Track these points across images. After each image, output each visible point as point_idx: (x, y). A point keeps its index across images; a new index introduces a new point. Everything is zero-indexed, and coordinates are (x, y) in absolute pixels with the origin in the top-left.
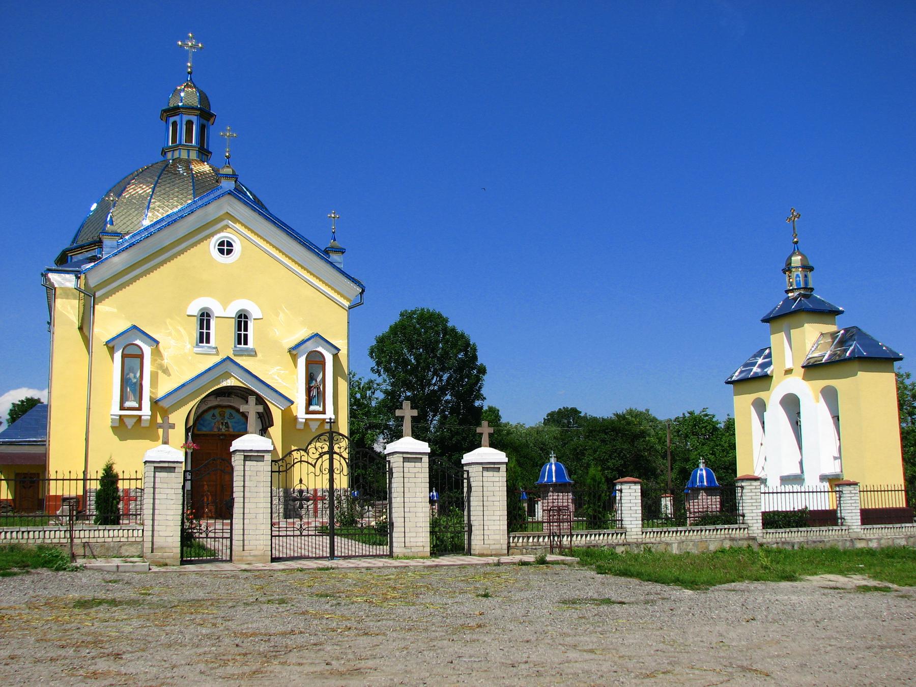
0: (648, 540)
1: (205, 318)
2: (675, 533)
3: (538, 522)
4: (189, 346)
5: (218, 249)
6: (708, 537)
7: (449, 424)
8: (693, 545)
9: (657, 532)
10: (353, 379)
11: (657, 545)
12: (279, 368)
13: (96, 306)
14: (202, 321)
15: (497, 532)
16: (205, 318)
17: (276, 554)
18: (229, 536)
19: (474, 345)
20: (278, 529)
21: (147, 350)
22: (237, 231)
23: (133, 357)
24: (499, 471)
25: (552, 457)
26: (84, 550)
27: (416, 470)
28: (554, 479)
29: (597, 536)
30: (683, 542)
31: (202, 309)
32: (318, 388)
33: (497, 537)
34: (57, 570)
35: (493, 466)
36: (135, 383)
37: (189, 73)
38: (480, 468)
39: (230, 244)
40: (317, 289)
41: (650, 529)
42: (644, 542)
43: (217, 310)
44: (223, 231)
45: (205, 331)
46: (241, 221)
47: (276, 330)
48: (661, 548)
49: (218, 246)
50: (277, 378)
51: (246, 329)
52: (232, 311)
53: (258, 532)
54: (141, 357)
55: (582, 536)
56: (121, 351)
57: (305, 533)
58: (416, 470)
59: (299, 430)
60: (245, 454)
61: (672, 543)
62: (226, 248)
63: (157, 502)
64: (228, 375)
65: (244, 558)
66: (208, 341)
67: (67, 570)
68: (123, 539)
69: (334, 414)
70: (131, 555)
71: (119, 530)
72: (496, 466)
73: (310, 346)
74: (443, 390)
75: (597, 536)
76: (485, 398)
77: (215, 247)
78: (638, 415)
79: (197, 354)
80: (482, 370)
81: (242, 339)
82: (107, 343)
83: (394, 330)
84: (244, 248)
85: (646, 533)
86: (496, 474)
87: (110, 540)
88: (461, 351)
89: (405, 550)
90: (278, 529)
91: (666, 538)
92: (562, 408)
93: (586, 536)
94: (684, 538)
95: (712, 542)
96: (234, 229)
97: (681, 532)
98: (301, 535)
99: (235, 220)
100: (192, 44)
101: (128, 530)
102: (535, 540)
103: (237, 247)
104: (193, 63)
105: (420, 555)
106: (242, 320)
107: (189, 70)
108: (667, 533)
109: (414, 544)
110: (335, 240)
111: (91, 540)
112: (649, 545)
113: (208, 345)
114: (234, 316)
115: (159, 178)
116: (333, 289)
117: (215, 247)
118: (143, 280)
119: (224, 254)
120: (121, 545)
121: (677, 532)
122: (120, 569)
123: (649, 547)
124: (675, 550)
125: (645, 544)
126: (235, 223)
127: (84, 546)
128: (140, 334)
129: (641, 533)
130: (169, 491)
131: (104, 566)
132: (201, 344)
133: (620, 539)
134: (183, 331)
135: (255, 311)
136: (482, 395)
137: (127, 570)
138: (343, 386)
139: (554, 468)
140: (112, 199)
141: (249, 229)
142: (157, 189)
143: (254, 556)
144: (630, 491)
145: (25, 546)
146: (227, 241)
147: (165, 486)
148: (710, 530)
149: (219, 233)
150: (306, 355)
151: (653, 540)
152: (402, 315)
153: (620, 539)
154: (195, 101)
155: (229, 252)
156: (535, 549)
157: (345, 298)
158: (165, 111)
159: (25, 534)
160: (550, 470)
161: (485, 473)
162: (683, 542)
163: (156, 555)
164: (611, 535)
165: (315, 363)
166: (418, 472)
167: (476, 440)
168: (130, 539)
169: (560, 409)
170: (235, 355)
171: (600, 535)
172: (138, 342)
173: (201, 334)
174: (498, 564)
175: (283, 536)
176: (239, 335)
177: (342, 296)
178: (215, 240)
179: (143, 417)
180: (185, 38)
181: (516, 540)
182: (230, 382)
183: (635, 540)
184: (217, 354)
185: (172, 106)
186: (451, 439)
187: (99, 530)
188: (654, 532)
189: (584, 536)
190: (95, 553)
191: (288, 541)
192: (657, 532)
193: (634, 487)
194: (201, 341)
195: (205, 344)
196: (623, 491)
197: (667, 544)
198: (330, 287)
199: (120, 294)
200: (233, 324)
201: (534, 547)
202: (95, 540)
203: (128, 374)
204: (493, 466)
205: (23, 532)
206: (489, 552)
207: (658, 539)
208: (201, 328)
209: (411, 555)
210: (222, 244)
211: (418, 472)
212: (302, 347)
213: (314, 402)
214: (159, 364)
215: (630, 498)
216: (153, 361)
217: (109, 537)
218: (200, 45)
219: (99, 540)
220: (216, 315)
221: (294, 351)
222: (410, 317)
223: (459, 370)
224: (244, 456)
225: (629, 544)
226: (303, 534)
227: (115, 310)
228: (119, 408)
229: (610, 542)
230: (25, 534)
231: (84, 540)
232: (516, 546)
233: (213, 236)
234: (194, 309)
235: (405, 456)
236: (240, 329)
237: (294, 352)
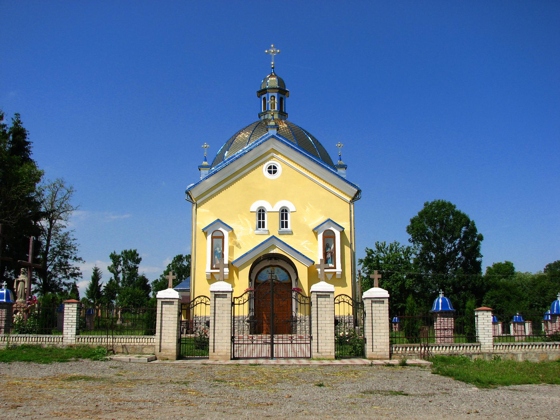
0: (498, 351)
1: (261, 213)
2: (448, 348)
3: (510, 336)
4: (251, 230)
5: (268, 171)
6: (548, 350)
7: (458, 273)
8: (535, 356)
9: (506, 346)
10: (398, 247)
11: (505, 355)
12: (307, 241)
13: (197, 209)
14: (259, 215)
15: (383, 344)
16: (261, 213)
17: (237, 355)
18: (309, 342)
19: (473, 222)
20: (277, 339)
21: (226, 233)
22: (279, 159)
23: (218, 238)
24: (384, 303)
25: (441, 293)
26: (123, 349)
27: (326, 303)
28: (440, 308)
29: (458, 347)
30: (527, 353)
31: (282, 207)
32: (331, 253)
33: (383, 347)
34: (94, 360)
35: (379, 300)
36: (220, 254)
37: (272, 68)
38: (370, 301)
39: (275, 167)
40: (330, 191)
41: (500, 344)
42: (495, 352)
43: (268, 207)
44: (270, 160)
45: (261, 221)
46: (281, 153)
47: (305, 218)
48: (509, 357)
49: (268, 169)
50: (306, 248)
51: (286, 218)
52: (277, 208)
53: (223, 341)
54: (223, 238)
55: (446, 347)
56: (211, 235)
57: (294, 342)
58: (326, 303)
59: (338, 279)
60: (215, 293)
61: (517, 354)
62: (272, 170)
63: (163, 322)
64: (274, 247)
65: (214, 357)
66: (264, 227)
67: (100, 360)
68: (145, 344)
69: (341, 269)
70: (149, 353)
71: (142, 338)
72: (381, 300)
73: (326, 227)
74: (456, 252)
75: (458, 347)
76: (482, 256)
77: (266, 170)
78: (500, 263)
79: (256, 234)
80: (481, 238)
81: (284, 224)
82: (203, 230)
83: (422, 215)
84: (283, 170)
85: (497, 346)
86: (381, 305)
87: (138, 344)
88: (463, 226)
89: (317, 354)
90: (277, 339)
91: (513, 350)
92: (556, 261)
93: (450, 347)
94: (527, 350)
95: (551, 354)
96: (277, 158)
97: (525, 346)
98: (252, 344)
99: (277, 153)
100: (274, 51)
101: (140, 338)
102: (412, 349)
103: (279, 169)
104: (275, 61)
105: (328, 358)
106: (284, 213)
107: (272, 66)
108: (514, 346)
109: (324, 351)
110: (341, 160)
111: (127, 344)
112: (499, 355)
113: (263, 229)
114: (255, 211)
115: (253, 132)
116: (340, 190)
117: (266, 170)
118: (224, 192)
119: (271, 174)
120: (143, 347)
121: (522, 346)
122: (131, 361)
123: (498, 356)
124: (520, 359)
125: (495, 354)
126: (278, 155)
127: (123, 347)
128: (222, 224)
129: (492, 346)
130: (170, 316)
131: (123, 359)
132: (259, 229)
133: (476, 350)
134: (246, 220)
135: (291, 207)
136: (480, 254)
137: (135, 362)
138: (347, 250)
139: (440, 301)
140: (205, 146)
141: (286, 158)
142: (252, 138)
143: (220, 356)
144: (483, 316)
145: (91, 347)
146: (273, 166)
147: (168, 313)
148: (550, 345)
149: (268, 161)
150: (323, 233)
151: (502, 351)
152: (425, 205)
153: (476, 350)
154: (276, 85)
155: (275, 172)
156: (411, 355)
157: (348, 196)
158: (259, 92)
159: (92, 339)
160: (438, 302)
161: (374, 305)
162: (527, 353)
163: (162, 354)
164: (468, 347)
165: (329, 237)
166: (327, 304)
167: (476, 283)
168: (149, 344)
169: (555, 262)
170: (280, 234)
171: (460, 347)
172: (221, 229)
173: (259, 223)
174: (372, 365)
175: (246, 344)
176: (282, 222)
177: (346, 194)
178: (265, 166)
179: (337, 273)
180: (276, 47)
181: (397, 349)
182: (276, 251)
183: (488, 351)
184: (269, 234)
185: (262, 88)
186: (459, 283)
187: (132, 338)
188: (503, 346)
189: (448, 347)
190: (129, 352)
191: (187, 347)
192: (506, 346)
193: (486, 313)
194: (260, 227)
195: (262, 229)
196: (479, 316)
197: (513, 354)
198: (338, 189)
199: (211, 201)
200: (277, 216)
201: (410, 354)
202: (129, 344)
203: (216, 248)
204: (379, 300)
205: (91, 338)
206: (376, 357)
207: (506, 351)
208: (260, 219)
209: (322, 357)
210: (270, 167)
211: (327, 304)
212: (320, 227)
213: (329, 262)
214: (234, 242)
215: (483, 321)
216: (231, 240)
217: (137, 342)
218: (278, 51)
219: (131, 344)
220: (291, 211)
221: (316, 231)
222: (431, 206)
223: (465, 237)
224: (215, 294)
225: (482, 353)
226: (293, 342)
227: (208, 211)
228: (210, 268)
229: (468, 352)
230: (92, 339)
231: (123, 344)
232: (397, 353)
233: (265, 164)
234: (254, 207)
235: (318, 294)
236: (283, 219)
237: (315, 231)
